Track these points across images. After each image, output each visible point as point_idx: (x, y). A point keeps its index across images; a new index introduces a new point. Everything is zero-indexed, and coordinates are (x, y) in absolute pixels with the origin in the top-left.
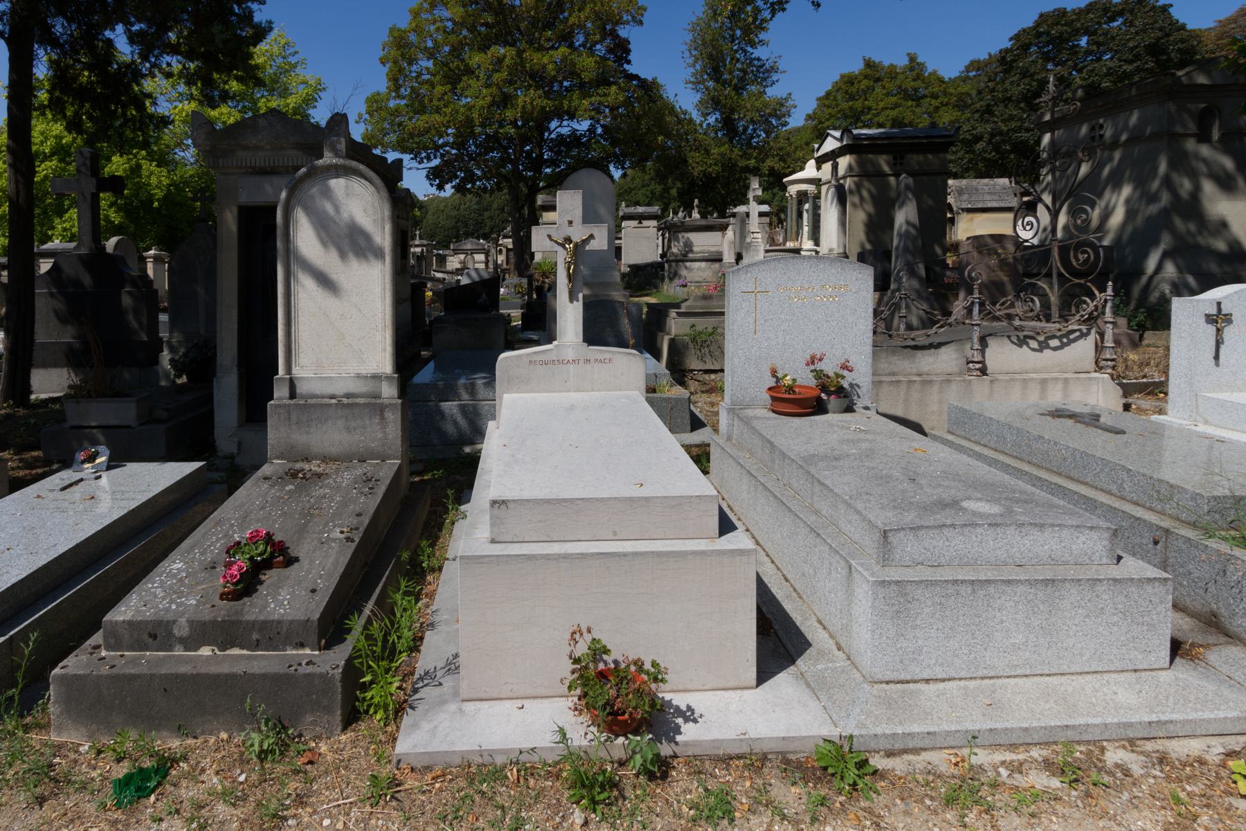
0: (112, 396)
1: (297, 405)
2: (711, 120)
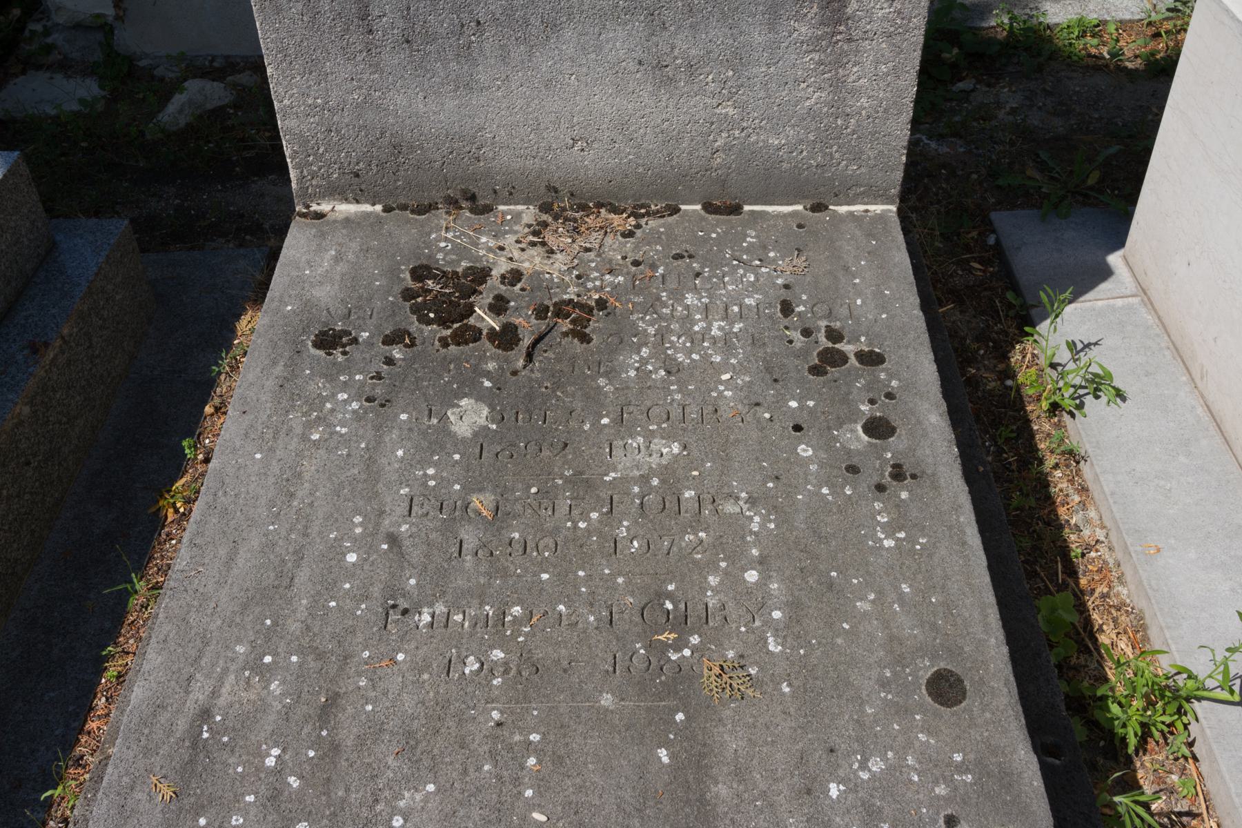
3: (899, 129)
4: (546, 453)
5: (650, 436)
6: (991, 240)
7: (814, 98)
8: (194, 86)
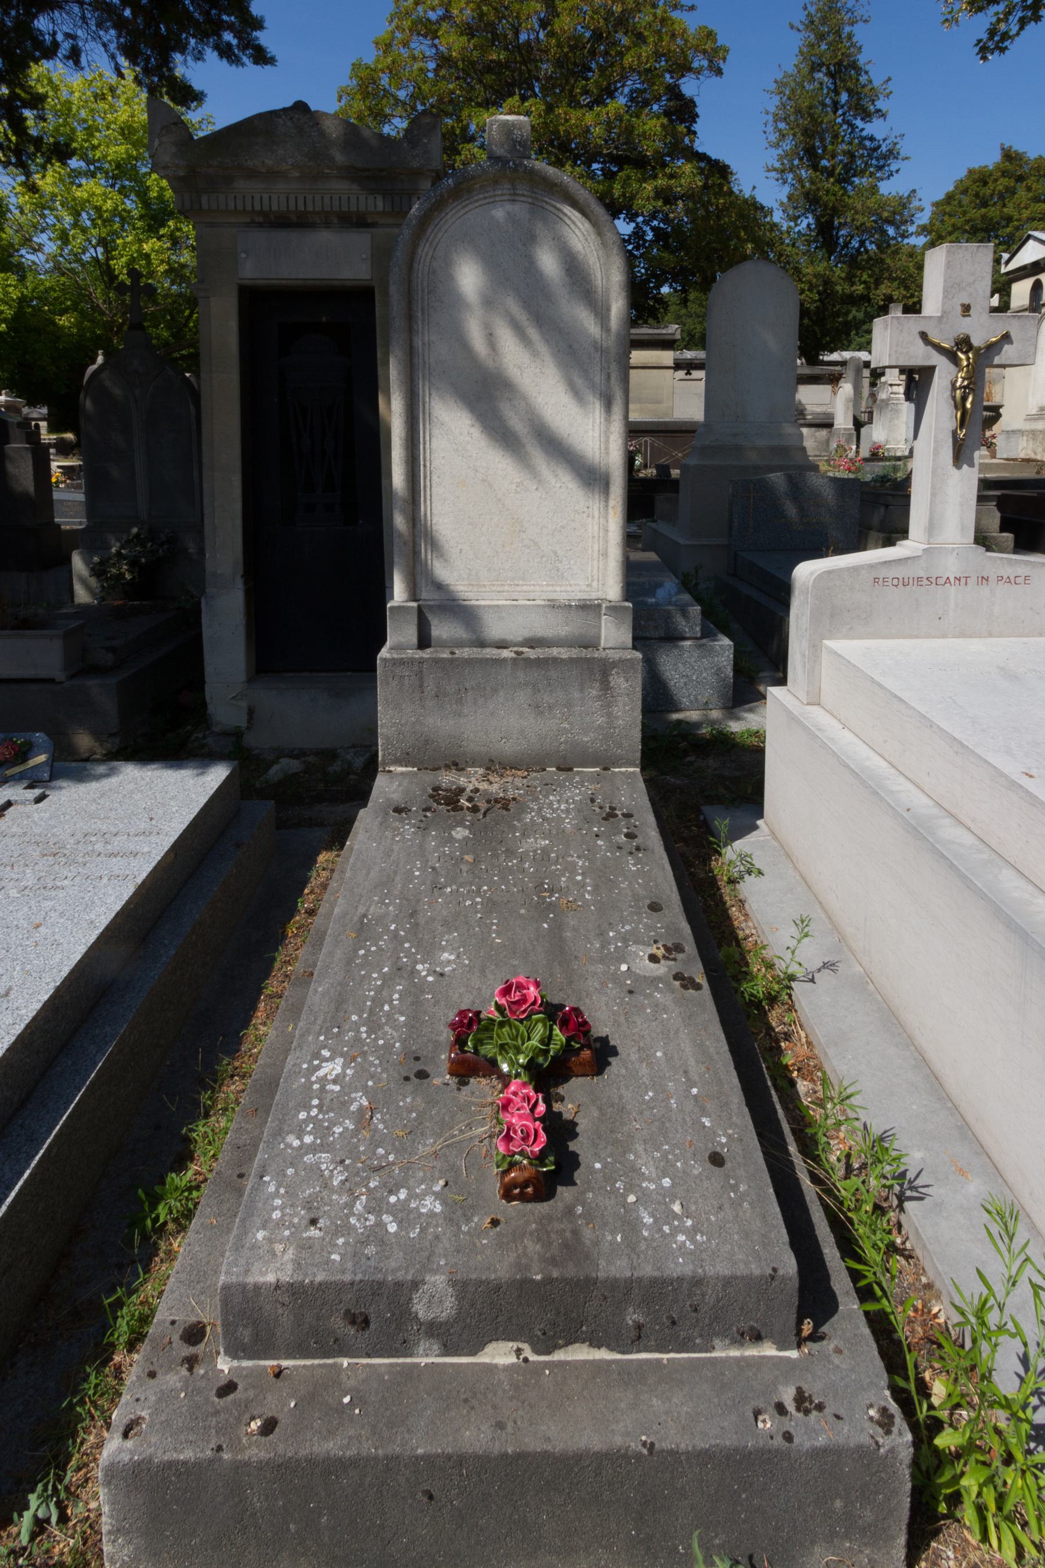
0: (14, 628)
1: (437, 661)
2: (803, 224)
3: (637, 734)
4: (494, 844)
5: (536, 839)
6: (702, 818)
7: (601, 720)
8: (284, 761)
